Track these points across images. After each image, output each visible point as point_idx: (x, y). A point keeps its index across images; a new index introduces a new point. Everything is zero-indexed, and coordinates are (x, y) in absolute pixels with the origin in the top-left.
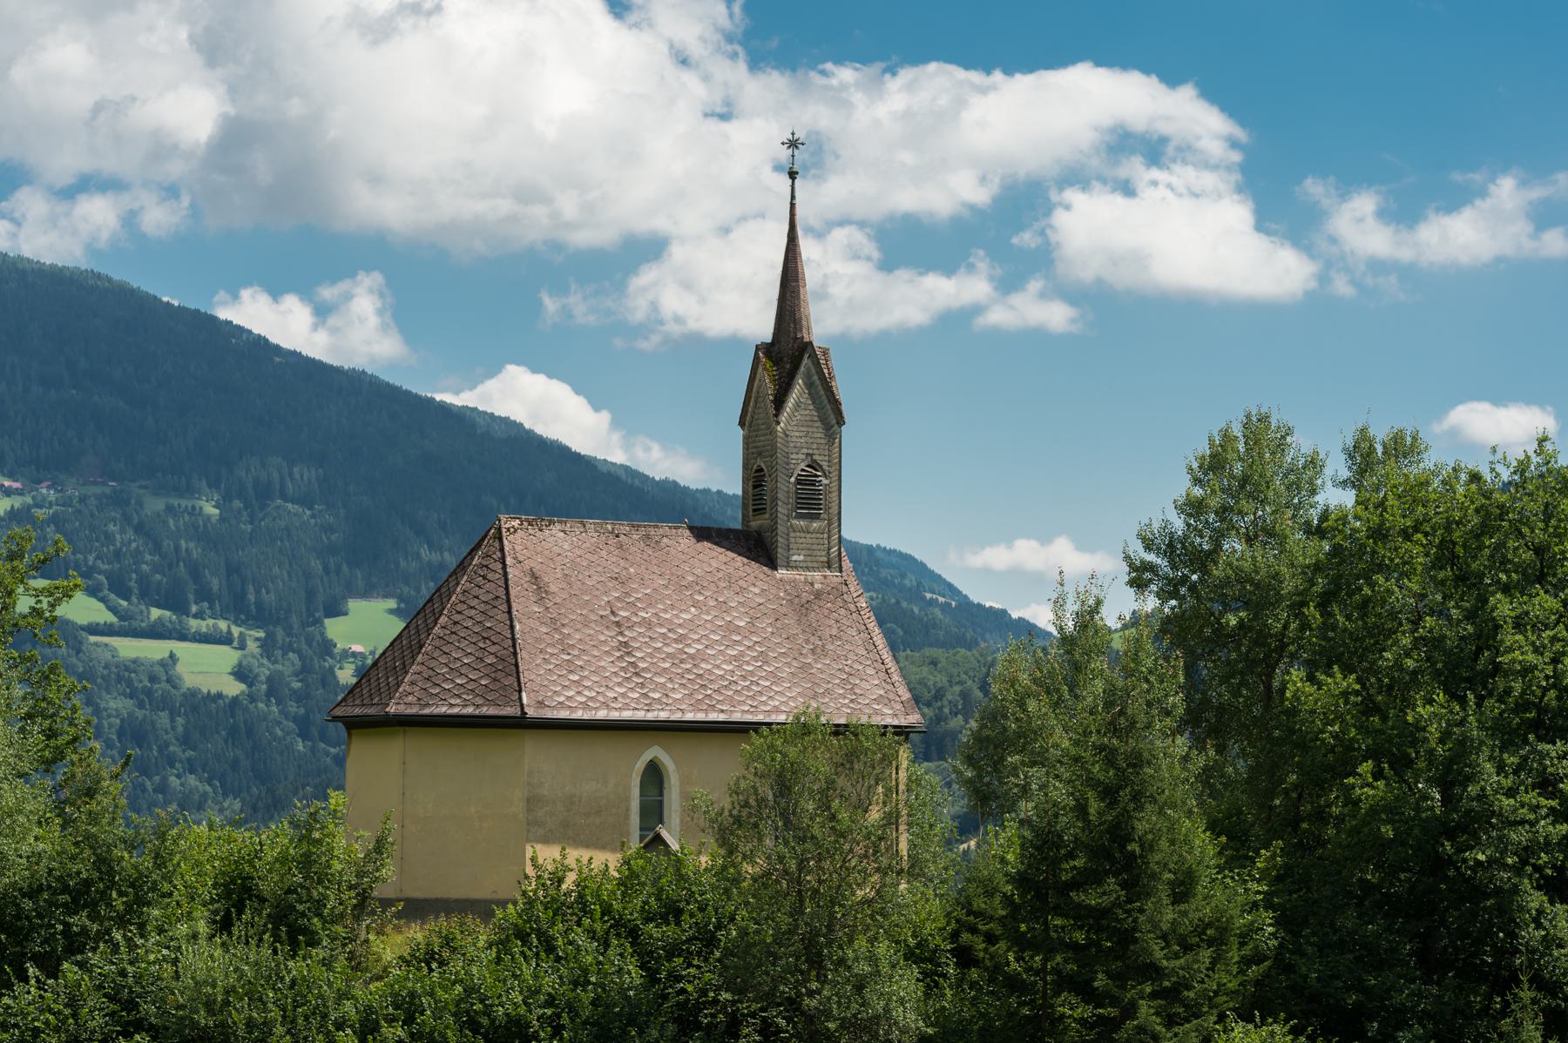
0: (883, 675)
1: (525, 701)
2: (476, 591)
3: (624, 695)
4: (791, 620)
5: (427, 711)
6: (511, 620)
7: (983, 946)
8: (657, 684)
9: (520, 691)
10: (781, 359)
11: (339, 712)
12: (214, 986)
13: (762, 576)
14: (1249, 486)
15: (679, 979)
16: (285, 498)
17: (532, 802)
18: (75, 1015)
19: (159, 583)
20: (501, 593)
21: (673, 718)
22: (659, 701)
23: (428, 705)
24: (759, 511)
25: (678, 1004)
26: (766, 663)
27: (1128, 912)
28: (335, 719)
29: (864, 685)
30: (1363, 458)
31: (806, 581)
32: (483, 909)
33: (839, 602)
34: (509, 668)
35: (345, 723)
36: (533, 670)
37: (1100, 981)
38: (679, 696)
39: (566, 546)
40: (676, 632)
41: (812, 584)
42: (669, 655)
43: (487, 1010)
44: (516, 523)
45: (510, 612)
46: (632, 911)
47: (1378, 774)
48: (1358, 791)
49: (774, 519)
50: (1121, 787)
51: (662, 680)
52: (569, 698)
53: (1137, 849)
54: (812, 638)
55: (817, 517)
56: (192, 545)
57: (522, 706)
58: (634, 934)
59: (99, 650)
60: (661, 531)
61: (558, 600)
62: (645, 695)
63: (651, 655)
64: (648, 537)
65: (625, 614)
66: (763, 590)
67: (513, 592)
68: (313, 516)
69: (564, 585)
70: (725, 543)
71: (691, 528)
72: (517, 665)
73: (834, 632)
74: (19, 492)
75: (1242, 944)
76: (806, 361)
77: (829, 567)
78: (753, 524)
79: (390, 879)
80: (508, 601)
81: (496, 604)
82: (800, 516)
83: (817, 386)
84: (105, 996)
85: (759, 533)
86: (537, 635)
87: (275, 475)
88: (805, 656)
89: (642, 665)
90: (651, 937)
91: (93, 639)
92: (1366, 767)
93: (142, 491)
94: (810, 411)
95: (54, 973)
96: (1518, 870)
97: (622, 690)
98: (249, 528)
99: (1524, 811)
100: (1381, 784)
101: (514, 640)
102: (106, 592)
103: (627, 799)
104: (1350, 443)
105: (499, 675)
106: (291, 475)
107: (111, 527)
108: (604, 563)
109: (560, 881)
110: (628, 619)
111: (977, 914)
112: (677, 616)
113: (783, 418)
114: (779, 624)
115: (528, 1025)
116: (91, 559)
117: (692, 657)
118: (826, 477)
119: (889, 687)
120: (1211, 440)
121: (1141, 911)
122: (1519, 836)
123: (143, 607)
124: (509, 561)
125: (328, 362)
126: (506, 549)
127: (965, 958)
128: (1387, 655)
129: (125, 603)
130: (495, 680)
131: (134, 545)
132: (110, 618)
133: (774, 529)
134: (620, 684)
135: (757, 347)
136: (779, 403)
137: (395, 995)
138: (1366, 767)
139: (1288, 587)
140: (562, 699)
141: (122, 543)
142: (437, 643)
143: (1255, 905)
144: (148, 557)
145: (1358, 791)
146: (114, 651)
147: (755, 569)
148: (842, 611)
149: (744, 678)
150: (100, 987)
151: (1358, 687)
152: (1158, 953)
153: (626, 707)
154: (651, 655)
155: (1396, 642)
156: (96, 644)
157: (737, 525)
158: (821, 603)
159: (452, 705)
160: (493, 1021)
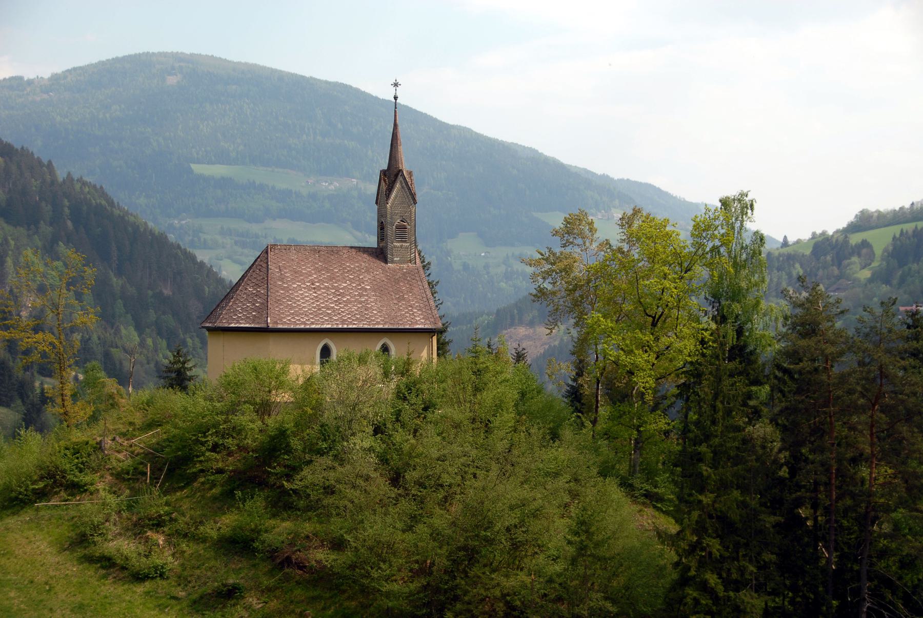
1: (269, 321)
3: (312, 318)
36: (273, 309)
40: (339, 292)
57: (267, 323)
65: (318, 284)
78: (381, 245)
111: (665, 320)
113: (390, 201)
153: (312, 323)
159: (241, 323)
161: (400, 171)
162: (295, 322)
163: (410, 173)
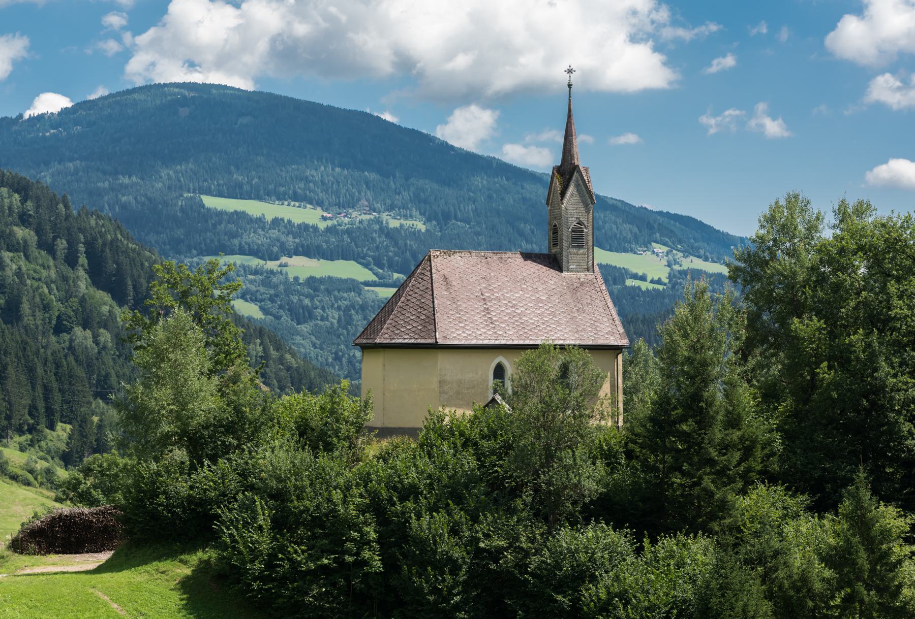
0: (611, 321)
1: (437, 336)
2: (418, 285)
3: (485, 333)
4: (568, 296)
5: (393, 341)
6: (433, 298)
7: (639, 450)
8: (501, 327)
9: (435, 332)
10: (565, 174)
11: (357, 342)
12: (280, 470)
13: (555, 276)
14: (786, 229)
15: (495, 465)
16: (456, 219)
17: (442, 383)
18: (223, 483)
19: (398, 261)
20: (430, 285)
21: (508, 343)
22: (502, 335)
23: (394, 338)
24: (555, 245)
25: (494, 477)
26: (554, 316)
27: (700, 435)
28: (356, 344)
29: (602, 326)
30: (843, 214)
31: (577, 278)
32: (412, 432)
33: (592, 287)
34: (431, 321)
35: (361, 347)
36: (442, 321)
37: (686, 467)
38: (511, 333)
39: (462, 263)
41: (579, 279)
42: (508, 313)
43: (401, 481)
44: (438, 253)
45: (433, 295)
46: (475, 434)
47: (830, 368)
48: (821, 376)
49: (561, 249)
50: (697, 376)
51: (504, 326)
52: (458, 335)
53: (704, 406)
54: (578, 305)
55: (582, 247)
56: (412, 243)
57: (436, 339)
58: (476, 444)
59: (369, 294)
60: (507, 255)
61: (456, 289)
62: (495, 332)
63: (499, 314)
64: (501, 258)
66: (555, 282)
67: (434, 286)
68: (470, 228)
69: (459, 282)
70: (538, 260)
71: (522, 254)
72: (434, 320)
73: (589, 301)
74: (331, 219)
75: (763, 449)
76: (575, 174)
77: (588, 271)
78: (553, 251)
79: (373, 418)
80: (432, 290)
81: (427, 291)
82: (575, 247)
83: (401, 226)
84: (238, 473)
85: (555, 255)
86: (445, 305)
87: (452, 208)
88: (574, 313)
89: (495, 318)
90: (483, 446)
91: (366, 288)
92: (825, 364)
93: (389, 217)
94: (577, 198)
95: (215, 462)
96: (899, 413)
97: (484, 331)
98: (440, 234)
99: (900, 384)
100: (832, 372)
101: (434, 308)
102: (372, 266)
103: (488, 381)
104: (836, 208)
105: (427, 324)
106: (459, 209)
107: (374, 235)
108: (479, 271)
109: (443, 421)
110: (489, 297)
111: (636, 435)
112: (513, 295)
113: (565, 201)
114: (562, 298)
115: (419, 488)
116: (365, 250)
117: (519, 314)
118: (586, 228)
119: (614, 327)
120: (770, 208)
121: (705, 434)
122: (900, 396)
123: (390, 273)
124: (434, 271)
125: (480, 154)
126: (433, 265)
127: (630, 455)
128: (843, 310)
129: (381, 271)
130: (424, 327)
131: (385, 243)
132: (375, 278)
133: (561, 254)
134: (483, 328)
135: (554, 169)
136: (563, 194)
137: (360, 473)
138: (825, 364)
139: (800, 277)
140: (455, 335)
141: (380, 242)
142: (400, 310)
143: (772, 430)
144: (392, 249)
145: (821, 376)
146: (376, 294)
147: (552, 272)
148: (593, 291)
149: (543, 324)
150: (235, 470)
151: (825, 326)
152: (714, 453)
154: (499, 314)
155: (848, 304)
156: (368, 291)
157: (545, 251)
158: (583, 288)
160: (403, 486)
161: (576, 168)
162: (466, 337)
163: (586, 170)
